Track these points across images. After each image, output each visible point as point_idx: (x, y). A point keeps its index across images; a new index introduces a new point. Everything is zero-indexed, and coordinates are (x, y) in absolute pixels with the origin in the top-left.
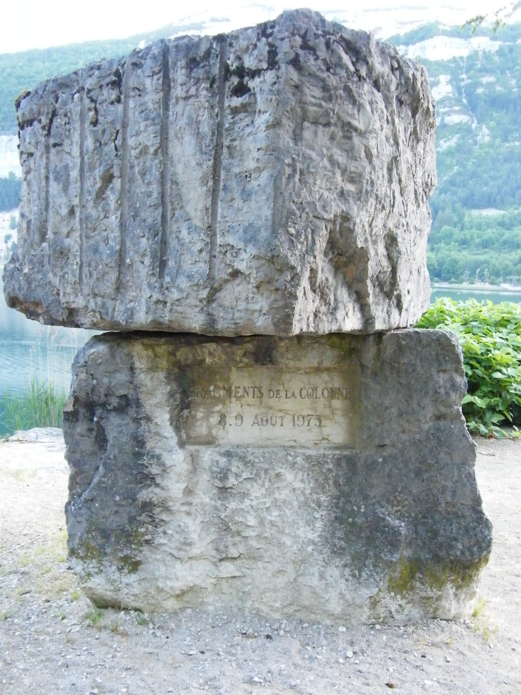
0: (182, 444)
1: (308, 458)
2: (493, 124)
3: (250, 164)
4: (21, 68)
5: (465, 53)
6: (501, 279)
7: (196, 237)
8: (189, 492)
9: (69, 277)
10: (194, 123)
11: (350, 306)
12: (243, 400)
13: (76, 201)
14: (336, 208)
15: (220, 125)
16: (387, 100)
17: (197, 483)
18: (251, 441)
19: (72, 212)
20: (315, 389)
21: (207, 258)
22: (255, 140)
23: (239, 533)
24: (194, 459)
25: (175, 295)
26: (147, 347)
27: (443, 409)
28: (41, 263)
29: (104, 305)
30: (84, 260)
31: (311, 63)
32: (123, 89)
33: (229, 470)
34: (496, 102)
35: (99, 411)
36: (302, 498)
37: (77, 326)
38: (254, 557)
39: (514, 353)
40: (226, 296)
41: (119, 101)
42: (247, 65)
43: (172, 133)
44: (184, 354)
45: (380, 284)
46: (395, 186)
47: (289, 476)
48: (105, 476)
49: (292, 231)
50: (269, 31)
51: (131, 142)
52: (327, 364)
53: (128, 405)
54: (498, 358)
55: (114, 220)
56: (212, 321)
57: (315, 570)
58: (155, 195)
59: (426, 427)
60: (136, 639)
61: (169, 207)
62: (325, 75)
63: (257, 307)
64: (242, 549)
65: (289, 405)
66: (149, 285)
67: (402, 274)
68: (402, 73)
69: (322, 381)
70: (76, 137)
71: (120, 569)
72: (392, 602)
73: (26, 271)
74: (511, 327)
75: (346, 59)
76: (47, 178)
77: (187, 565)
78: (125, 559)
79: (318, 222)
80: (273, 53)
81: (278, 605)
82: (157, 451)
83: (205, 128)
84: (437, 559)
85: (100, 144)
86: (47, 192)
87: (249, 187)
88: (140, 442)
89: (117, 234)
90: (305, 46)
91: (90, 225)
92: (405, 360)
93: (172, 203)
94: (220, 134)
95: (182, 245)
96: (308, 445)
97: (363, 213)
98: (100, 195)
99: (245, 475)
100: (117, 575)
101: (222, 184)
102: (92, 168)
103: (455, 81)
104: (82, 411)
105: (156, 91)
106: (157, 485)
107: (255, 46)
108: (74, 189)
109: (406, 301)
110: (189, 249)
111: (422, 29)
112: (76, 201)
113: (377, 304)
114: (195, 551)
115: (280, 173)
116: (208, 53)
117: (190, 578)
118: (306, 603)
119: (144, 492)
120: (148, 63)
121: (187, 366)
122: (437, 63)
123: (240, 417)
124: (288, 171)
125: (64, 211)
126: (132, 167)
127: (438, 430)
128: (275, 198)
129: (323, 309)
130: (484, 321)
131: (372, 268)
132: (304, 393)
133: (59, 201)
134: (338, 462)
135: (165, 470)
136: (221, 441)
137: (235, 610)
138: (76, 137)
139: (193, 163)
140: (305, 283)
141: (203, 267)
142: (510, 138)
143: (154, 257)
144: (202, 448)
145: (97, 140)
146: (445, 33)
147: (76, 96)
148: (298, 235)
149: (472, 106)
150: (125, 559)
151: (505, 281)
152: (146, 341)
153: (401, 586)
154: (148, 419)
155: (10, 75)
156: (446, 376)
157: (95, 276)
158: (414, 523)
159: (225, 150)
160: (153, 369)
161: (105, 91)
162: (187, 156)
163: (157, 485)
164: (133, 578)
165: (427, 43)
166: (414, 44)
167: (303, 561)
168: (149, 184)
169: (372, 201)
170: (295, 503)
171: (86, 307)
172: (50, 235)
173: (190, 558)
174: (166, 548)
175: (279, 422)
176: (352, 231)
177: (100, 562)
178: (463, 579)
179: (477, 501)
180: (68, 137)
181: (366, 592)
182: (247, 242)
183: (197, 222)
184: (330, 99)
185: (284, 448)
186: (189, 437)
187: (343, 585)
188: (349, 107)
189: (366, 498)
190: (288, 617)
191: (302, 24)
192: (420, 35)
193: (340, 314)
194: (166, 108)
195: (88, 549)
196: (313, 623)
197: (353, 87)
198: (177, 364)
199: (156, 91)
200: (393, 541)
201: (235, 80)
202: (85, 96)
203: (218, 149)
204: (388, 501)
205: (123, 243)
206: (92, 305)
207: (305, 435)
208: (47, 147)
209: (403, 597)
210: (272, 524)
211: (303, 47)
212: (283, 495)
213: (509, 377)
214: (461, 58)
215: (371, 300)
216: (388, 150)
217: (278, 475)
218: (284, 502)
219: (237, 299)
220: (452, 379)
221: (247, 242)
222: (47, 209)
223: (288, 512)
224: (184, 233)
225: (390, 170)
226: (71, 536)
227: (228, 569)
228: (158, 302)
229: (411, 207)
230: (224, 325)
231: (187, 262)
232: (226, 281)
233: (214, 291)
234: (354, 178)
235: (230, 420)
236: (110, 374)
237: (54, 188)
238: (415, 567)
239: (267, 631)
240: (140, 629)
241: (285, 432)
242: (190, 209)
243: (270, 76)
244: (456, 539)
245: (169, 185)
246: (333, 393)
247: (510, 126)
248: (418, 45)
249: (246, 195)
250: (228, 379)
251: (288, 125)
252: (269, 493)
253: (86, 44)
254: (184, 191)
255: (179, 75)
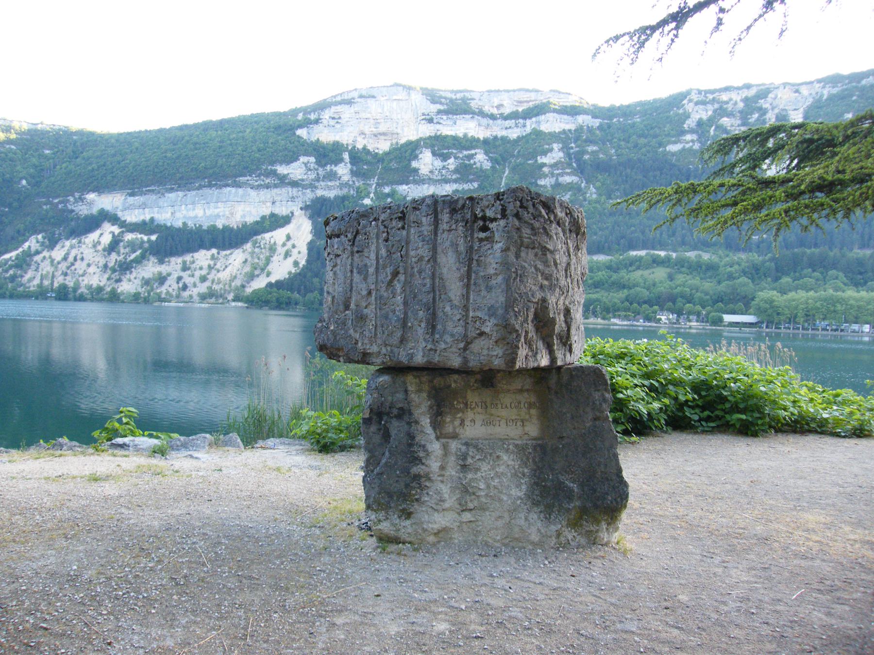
0: (437, 438)
1: (516, 446)
2: (598, 184)
3: (492, 271)
4: (198, 136)
5: (572, 127)
6: (611, 315)
7: (456, 312)
8: (442, 468)
9: (367, 333)
10: (455, 245)
11: (544, 351)
12: (475, 411)
13: (373, 287)
14: (539, 295)
15: (471, 247)
16: (564, 232)
17: (447, 463)
18: (480, 436)
19: (370, 293)
20: (520, 403)
21: (463, 324)
22: (494, 258)
23: (474, 494)
24: (445, 447)
25: (443, 346)
26: (415, 377)
27: (598, 414)
28: (344, 324)
29: (392, 351)
30: (378, 323)
31: (526, 216)
32: (406, 221)
33: (468, 454)
34: (601, 167)
35: (385, 418)
36: (513, 471)
37: (368, 364)
38: (483, 508)
39: (631, 379)
40: (476, 346)
41: (403, 228)
42: (488, 215)
43: (439, 250)
44: (438, 381)
45: (560, 338)
46: (569, 280)
47: (505, 457)
48: (390, 458)
49: (516, 309)
50: (501, 197)
51: (412, 253)
52: (527, 387)
53: (404, 413)
54: (620, 383)
55: (399, 299)
56: (466, 361)
57: (522, 515)
58: (428, 285)
59: (588, 425)
60: (413, 558)
61: (438, 293)
62: (533, 222)
63: (495, 353)
64: (476, 503)
65: (504, 413)
66: (425, 340)
67: (573, 331)
68: (572, 216)
69: (525, 398)
70: (373, 248)
71: (400, 517)
72: (569, 534)
73: (332, 328)
74: (627, 359)
75: (543, 211)
76: (352, 271)
77: (441, 515)
78: (403, 511)
79: (529, 304)
80: (504, 210)
81: (498, 538)
82: (423, 443)
83: (462, 248)
84: (596, 506)
85: (390, 253)
86: (352, 280)
87: (490, 284)
88: (413, 438)
89: (402, 307)
90: (522, 207)
91: (382, 302)
92: (575, 384)
93: (440, 291)
94: (471, 253)
95: (447, 316)
96: (516, 437)
97: (553, 297)
98: (390, 283)
99: (477, 457)
100: (398, 520)
101: (472, 282)
102: (385, 267)
103: (565, 149)
104: (375, 417)
105: (430, 225)
106: (423, 464)
107: (493, 205)
108: (372, 279)
109: (574, 346)
110: (451, 319)
111: (536, 107)
112: (373, 287)
113: (558, 350)
114: (447, 505)
115: (510, 277)
116: (463, 206)
117: (443, 523)
118: (517, 536)
119: (415, 468)
120: (424, 208)
121: (440, 389)
122: (550, 134)
123: (473, 421)
124: (514, 275)
125: (364, 293)
126: (412, 268)
127: (595, 427)
128: (507, 291)
129: (530, 354)
130: (608, 355)
131: (557, 329)
132: (513, 405)
133: (360, 286)
134: (535, 448)
135: (428, 454)
136: (462, 436)
137: (472, 542)
138: (373, 248)
139: (455, 269)
140: (523, 340)
141: (460, 329)
142: (612, 196)
143: (428, 323)
144: (450, 441)
145: (388, 251)
146: (555, 111)
147: (373, 223)
148: (519, 312)
149: (581, 170)
150: (403, 511)
151: (614, 317)
152: (415, 373)
153: (574, 524)
154: (417, 422)
155: (188, 142)
156: (600, 394)
157: (386, 333)
158: (582, 485)
159: (475, 262)
160: (419, 391)
161: (394, 222)
162: (449, 265)
163: (423, 464)
164: (408, 522)
165: (542, 118)
166: (530, 118)
167: (515, 510)
168: (424, 278)
169: (558, 290)
170: (509, 474)
171: (379, 352)
172: (352, 306)
173: (443, 510)
174: (428, 503)
175: (498, 423)
176: (547, 308)
177: (387, 513)
178: (612, 519)
179: (620, 470)
180: (368, 247)
181: (553, 528)
182: (490, 316)
183: (456, 302)
184: (535, 235)
185: (500, 439)
186: (441, 434)
187: (539, 524)
188: (545, 238)
189: (552, 470)
190: (505, 545)
191: (520, 195)
192: (535, 112)
193: (539, 356)
194: (436, 234)
195: (379, 504)
196: (520, 548)
197: (547, 227)
198: (434, 388)
199: (430, 225)
200: (570, 496)
201: (481, 223)
202: (380, 224)
203: (470, 261)
204: (566, 472)
205: (406, 314)
206: (384, 351)
207: (514, 432)
208: (352, 254)
209: (576, 531)
210: (495, 487)
211: (521, 207)
212: (501, 469)
213: (628, 396)
214: (570, 130)
215: (555, 347)
216: (565, 259)
217: (498, 457)
218: (502, 473)
219: (482, 349)
220: (603, 395)
221: (490, 316)
222: (351, 290)
223: (504, 479)
224: (448, 309)
225: (566, 271)
226: (368, 497)
227: (467, 516)
228: (431, 349)
229: (576, 289)
230: (473, 363)
231: (450, 326)
232: (475, 338)
233: (468, 344)
234: (548, 277)
235: (467, 423)
236: (393, 394)
237: (357, 278)
238: (583, 511)
239: (494, 553)
240: (414, 553)
241: (501, 430)
242: (452, 295)
243: (502, 223)
244: (607, 494)
245: (437, 280)
246: (531, 406)
247: (612, 186)
248: (534, 119)
249: (489, 289)
250: (465, 397)
251: (513, 249)
252: (493, 468)
253: (252, 116)
254: (447, 284)
255: (445, 217)
